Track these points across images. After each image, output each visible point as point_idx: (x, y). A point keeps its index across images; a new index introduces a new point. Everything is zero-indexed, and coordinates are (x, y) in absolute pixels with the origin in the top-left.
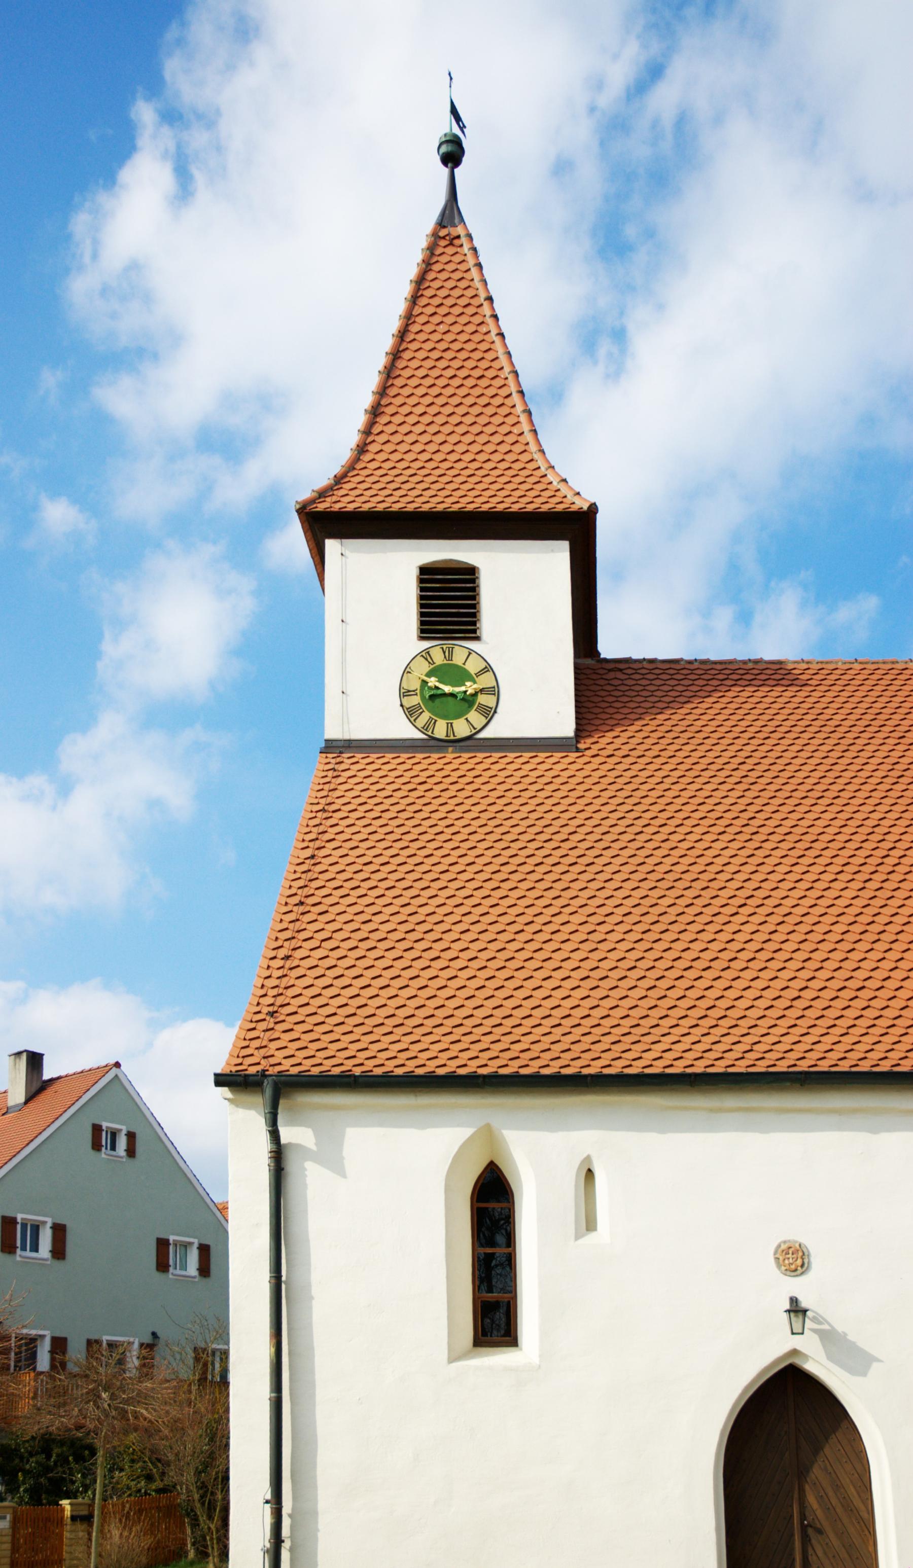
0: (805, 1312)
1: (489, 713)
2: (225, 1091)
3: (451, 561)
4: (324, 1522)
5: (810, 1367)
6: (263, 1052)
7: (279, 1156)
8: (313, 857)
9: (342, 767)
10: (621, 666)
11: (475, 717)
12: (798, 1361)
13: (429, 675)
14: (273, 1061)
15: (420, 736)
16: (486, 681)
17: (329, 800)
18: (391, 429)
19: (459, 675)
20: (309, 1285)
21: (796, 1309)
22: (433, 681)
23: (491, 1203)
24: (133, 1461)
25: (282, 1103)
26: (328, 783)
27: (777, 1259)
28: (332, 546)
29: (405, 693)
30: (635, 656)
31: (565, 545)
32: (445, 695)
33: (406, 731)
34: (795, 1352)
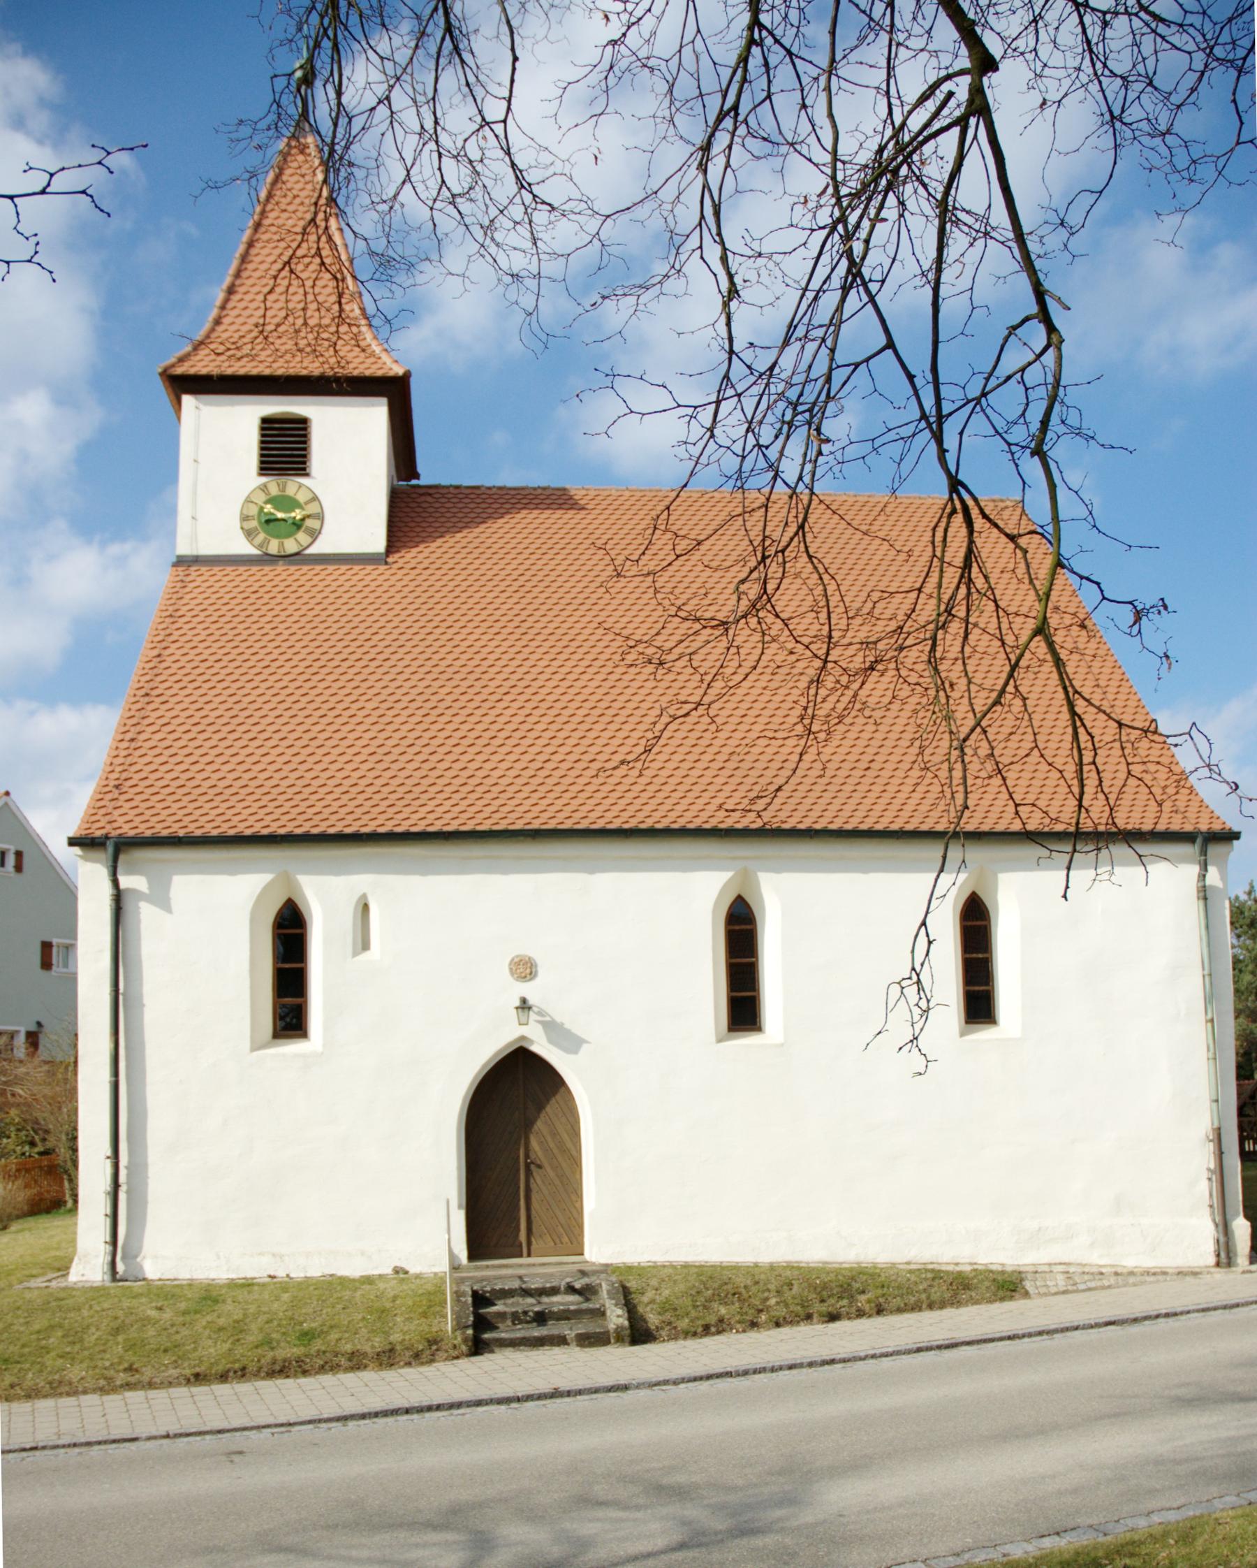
0: (530, 1008)
1: (315, 535)
2: (77, 850)
3: (287, 413)
4: (152, 1171)
5: (535, 1048)
6: (108, 818)
7: (118, 898)
8: (159, 656)
9: (189, 579)
10: (431, 491)
11: (302, 537)
12: (526, 1045)
13: (267, 502)
14: (115, 825)
15: (256, 552)
16: (312, 509)
17: (176, 607)
18: (243, 304)
19: (291, 504)
20: (141, 996)
21: (524, 1006)
22: (268, 508)
23: (290, 932)
24: (18, 1130)
25: (122, 858)
26: (177, 592)
27: (511, 969)
28: (188, 400)
29: (245, 518)
30: (444, 482)
31: (384, 400)
32: (277, 520)
33: (245, 548)
34: (523, 1038)
